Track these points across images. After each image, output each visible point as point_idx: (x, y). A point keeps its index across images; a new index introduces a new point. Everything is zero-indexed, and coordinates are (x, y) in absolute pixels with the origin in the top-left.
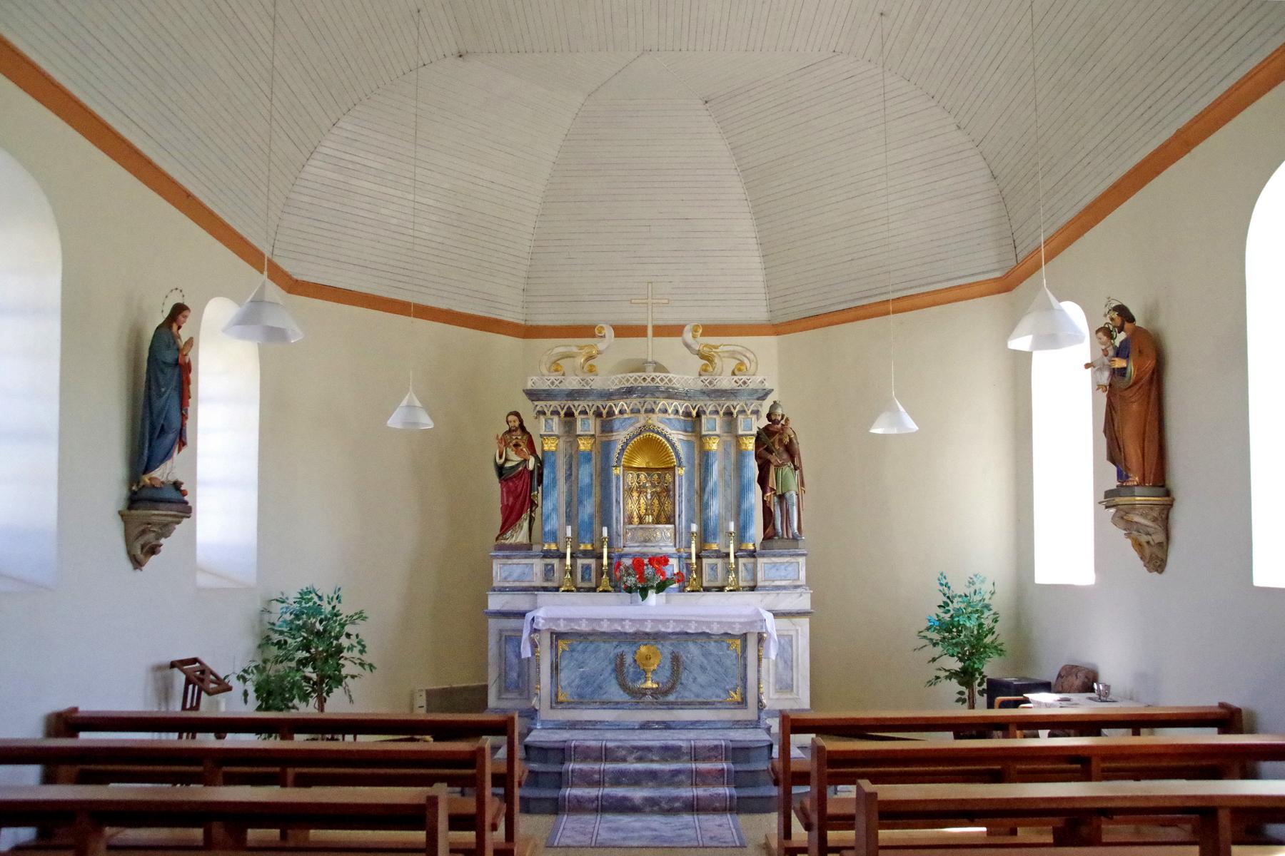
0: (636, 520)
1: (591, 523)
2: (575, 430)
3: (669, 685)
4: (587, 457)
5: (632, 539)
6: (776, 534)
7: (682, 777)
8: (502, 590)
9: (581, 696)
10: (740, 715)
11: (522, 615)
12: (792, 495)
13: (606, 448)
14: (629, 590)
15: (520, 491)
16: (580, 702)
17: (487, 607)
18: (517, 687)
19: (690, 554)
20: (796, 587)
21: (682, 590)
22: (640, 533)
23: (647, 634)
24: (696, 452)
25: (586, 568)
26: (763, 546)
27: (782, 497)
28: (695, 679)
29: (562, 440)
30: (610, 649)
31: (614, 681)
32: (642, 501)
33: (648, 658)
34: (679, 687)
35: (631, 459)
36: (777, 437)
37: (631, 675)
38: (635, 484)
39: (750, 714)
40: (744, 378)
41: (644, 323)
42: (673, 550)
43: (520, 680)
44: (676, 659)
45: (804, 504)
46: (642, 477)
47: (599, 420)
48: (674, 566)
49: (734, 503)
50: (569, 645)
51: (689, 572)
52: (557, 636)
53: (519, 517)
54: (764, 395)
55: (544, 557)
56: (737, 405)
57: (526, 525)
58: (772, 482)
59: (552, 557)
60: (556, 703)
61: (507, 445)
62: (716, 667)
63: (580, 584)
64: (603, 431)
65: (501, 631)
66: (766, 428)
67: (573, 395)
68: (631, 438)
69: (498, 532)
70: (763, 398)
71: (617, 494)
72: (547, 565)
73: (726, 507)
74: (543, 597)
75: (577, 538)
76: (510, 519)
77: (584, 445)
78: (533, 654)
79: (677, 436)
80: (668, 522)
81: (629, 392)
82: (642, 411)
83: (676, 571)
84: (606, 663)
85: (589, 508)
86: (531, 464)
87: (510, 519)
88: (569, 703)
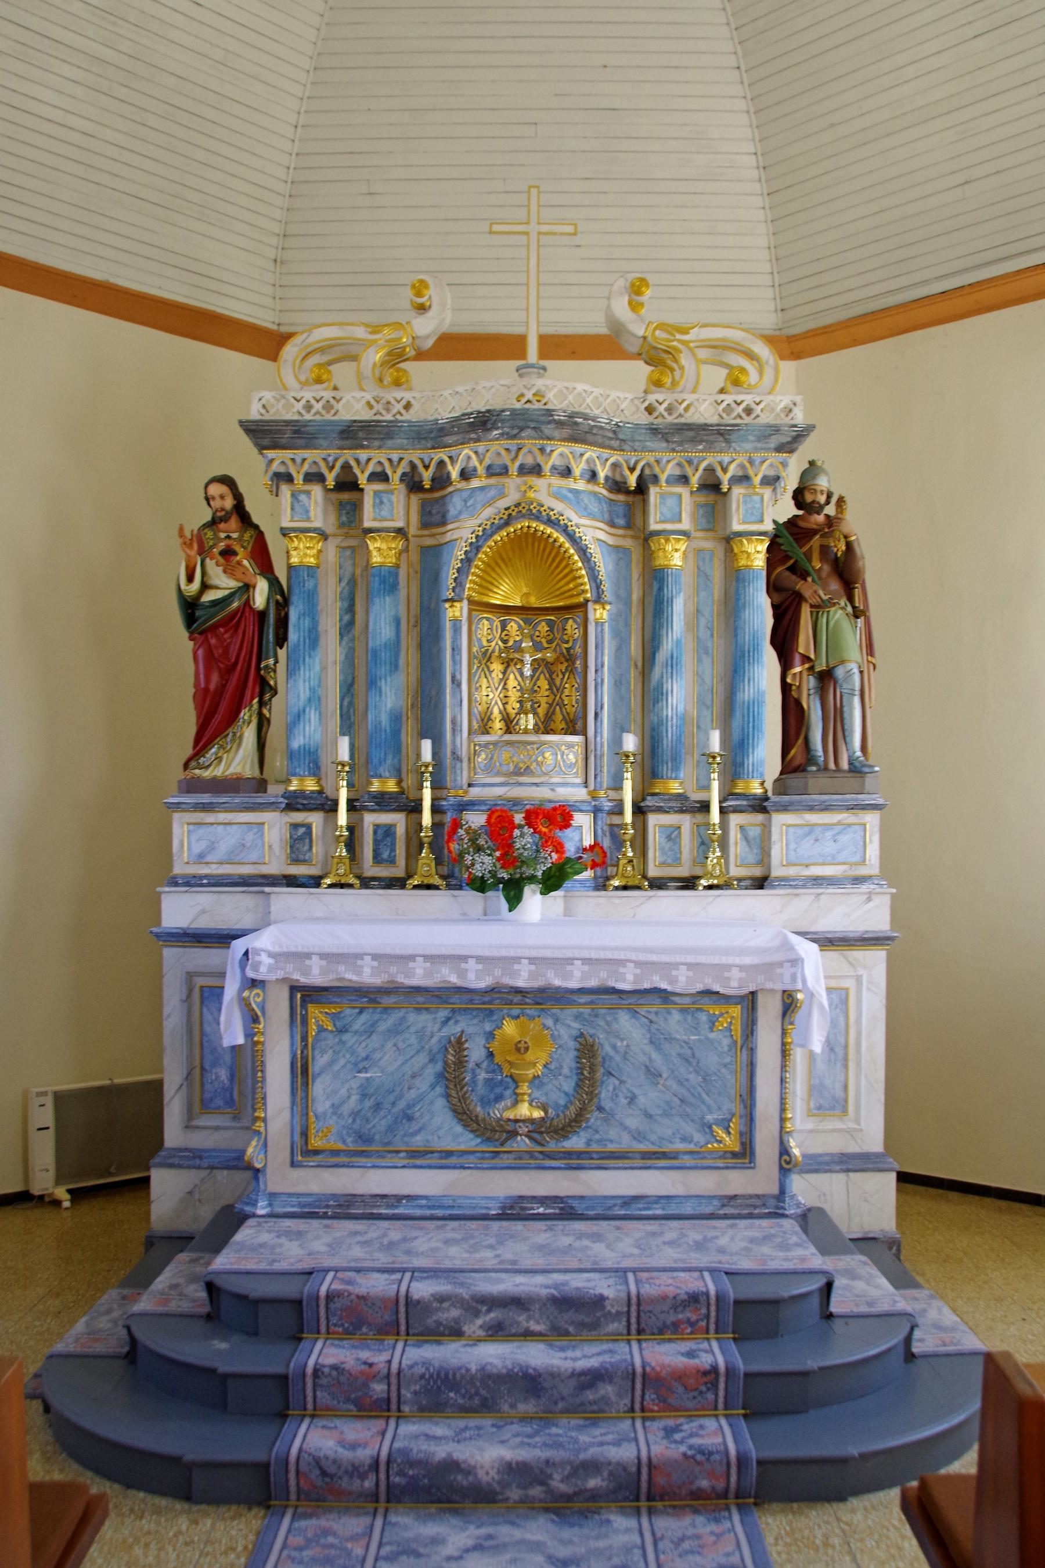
0: (498, 725)
1: (396, 733)
2: (361, 521)
3: (572, 1111)
4: (389, 580)
5: (489, 769)
6: (810, 759)
7: (607, 1390)
8: (192, 882)
9: (363, 1138)
10: (737, 1182)
11: (224, 938)
12: (851, 670)
13: (431, 559)
14: (480, 885)
15: (235, 656)
16: (363, 1150)
17: (158, 921)
18: (230, 1102)
19: (620, 803)
20: (858, 880)
21: (601, 885)
22: (505, 754)
23: (518, 991)
24: (635, 576)
25: (385, 833)
26: (781, 786)
27: (826, 678)
28: (632, 1099)
29: (332, 545)
30: (431, 1027)
31: (441, 1103)
32: (512, 682)
33: (520, 1048)
34: (594, 1118)
35: (486, 585)
36: (816, 541)
37: (481, 1089)
38: (497, 644)
39: (759, 1179)
40: (748, 399)
41: (519, 330)
42: (582, 794)
43: (230, 1086)
44: (587, 1051)
45: (874, 697)
46: (513, 627)
47: (415, 499)
48: (583, 831)
49: (720, 689)
50: (334, 1017)
51: (618, 843)
52: (304, 995)
53: (232, 717)
54: (791, 441)
55: (290, 807)
56: (730, 461)
57: (249, 735)
58: (804, 643)
59: (306, 808)
60: (304, 1152)
61: (203, 551)
62: (683, 1071)
63: (370, 869)
64: (425, 525)
65: (190, 976)
66: (792, 522)
67: (354, 434)
68: (487, 535)
69: (190, 751)
70: (788, 448)
71: (457, 661)
72: (295, 826)
73: (701, 703)
74: (284, 899)
75: (359, 768)
76: (213, 723)
77: (381, 552)
78: (249, 1035)
79: (594, 533)
80: (571, 730)
81: (482, 423)
82: (514, 469)
83: (588, 841)
84: (422, 1058)
85: (391, 696)
86: (261, 595)
87: (213, 723)
88: (336, 1153)
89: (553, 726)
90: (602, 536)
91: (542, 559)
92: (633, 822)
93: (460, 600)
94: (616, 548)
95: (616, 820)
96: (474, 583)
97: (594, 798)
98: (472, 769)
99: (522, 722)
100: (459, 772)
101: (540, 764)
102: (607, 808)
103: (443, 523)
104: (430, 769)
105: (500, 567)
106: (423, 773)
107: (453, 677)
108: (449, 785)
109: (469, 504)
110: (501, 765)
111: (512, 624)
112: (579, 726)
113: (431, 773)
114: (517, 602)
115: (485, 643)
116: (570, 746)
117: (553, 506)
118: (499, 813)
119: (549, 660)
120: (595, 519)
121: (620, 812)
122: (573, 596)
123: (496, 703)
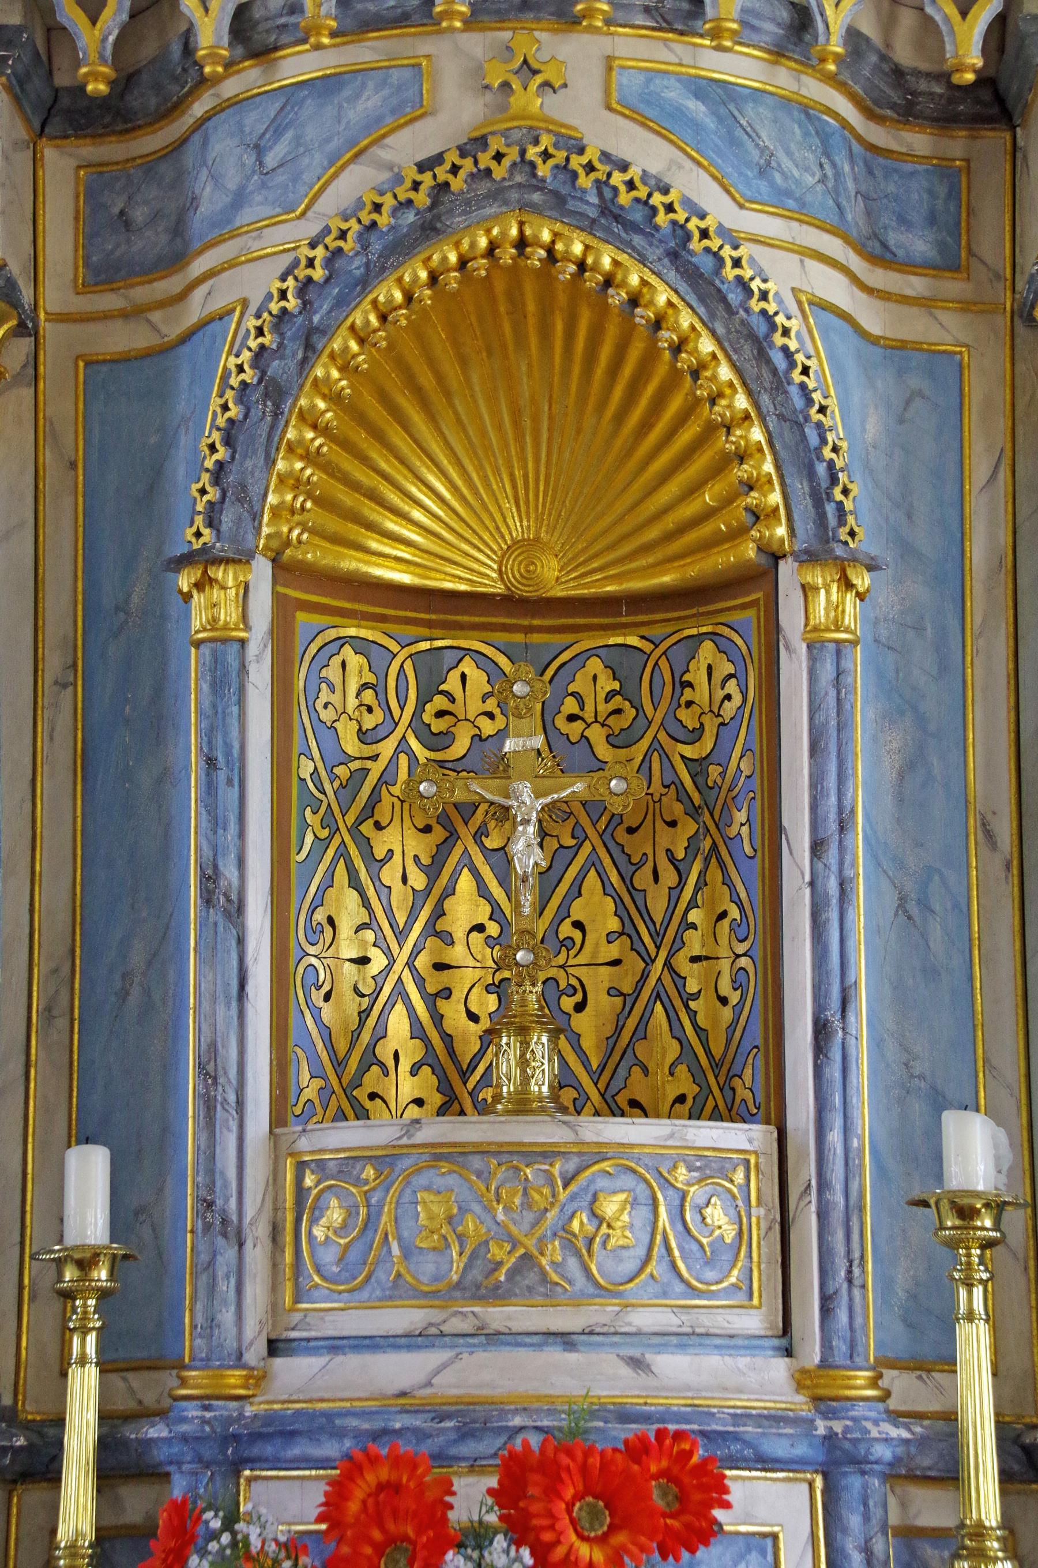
32: (465, 908)
35: (348, 507)
42: (765, 1383)
46: (470, 684)
47: (61, 163)
64: (102, 272)
80: (714, 1096)
89: (638, 1087)
90: (835, 289)
91: (582, 398)
92: (1007, 1522)
93: (242, 558)
94: (897, 350)
95: (930, 1509)
96: (297, 484)
97: (825, 1404)
98: (291, 1275)
99: (507, 1065)
100: (226, 1287)
101: (579, 1248)
102: (883, 1452)
103: (176, 259)
104: (102, 1274)
105: (406, 426)
106: (68, 1295)
107: (210, 878)
108: (189, 1345)
109: (271, 160)
110: (407, 1253)
111: (467, 666)
112: (749, 1083)
113: (104, 1295)
114: (476, 571)
115: (351, 745)
116: (711, 1166)
117: (622, 150)
118: (384, 1473)
119: (616, 806)
120: (800, 212)
121: (951, 1475)
122: (716, 541)
123: (400, 992)
